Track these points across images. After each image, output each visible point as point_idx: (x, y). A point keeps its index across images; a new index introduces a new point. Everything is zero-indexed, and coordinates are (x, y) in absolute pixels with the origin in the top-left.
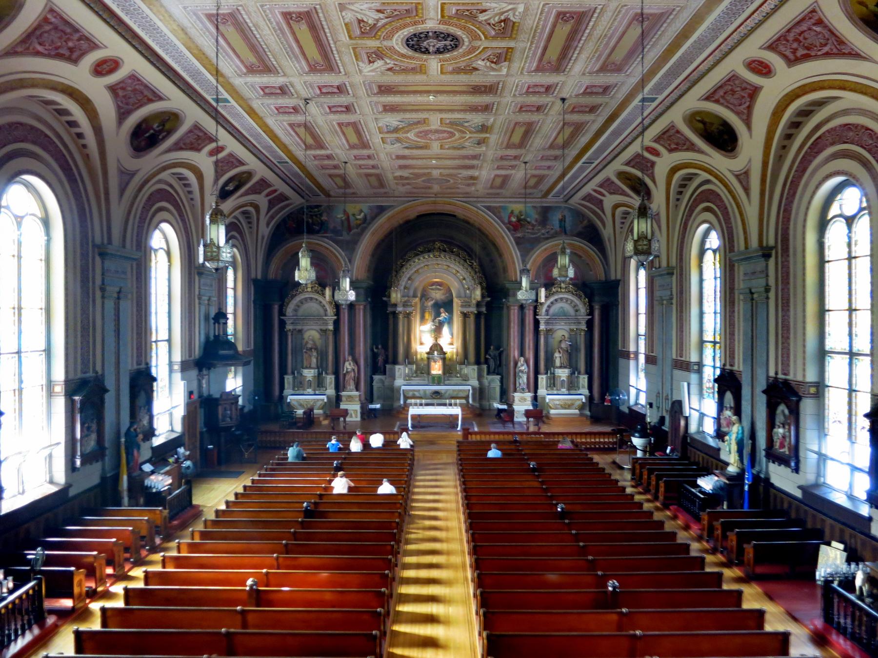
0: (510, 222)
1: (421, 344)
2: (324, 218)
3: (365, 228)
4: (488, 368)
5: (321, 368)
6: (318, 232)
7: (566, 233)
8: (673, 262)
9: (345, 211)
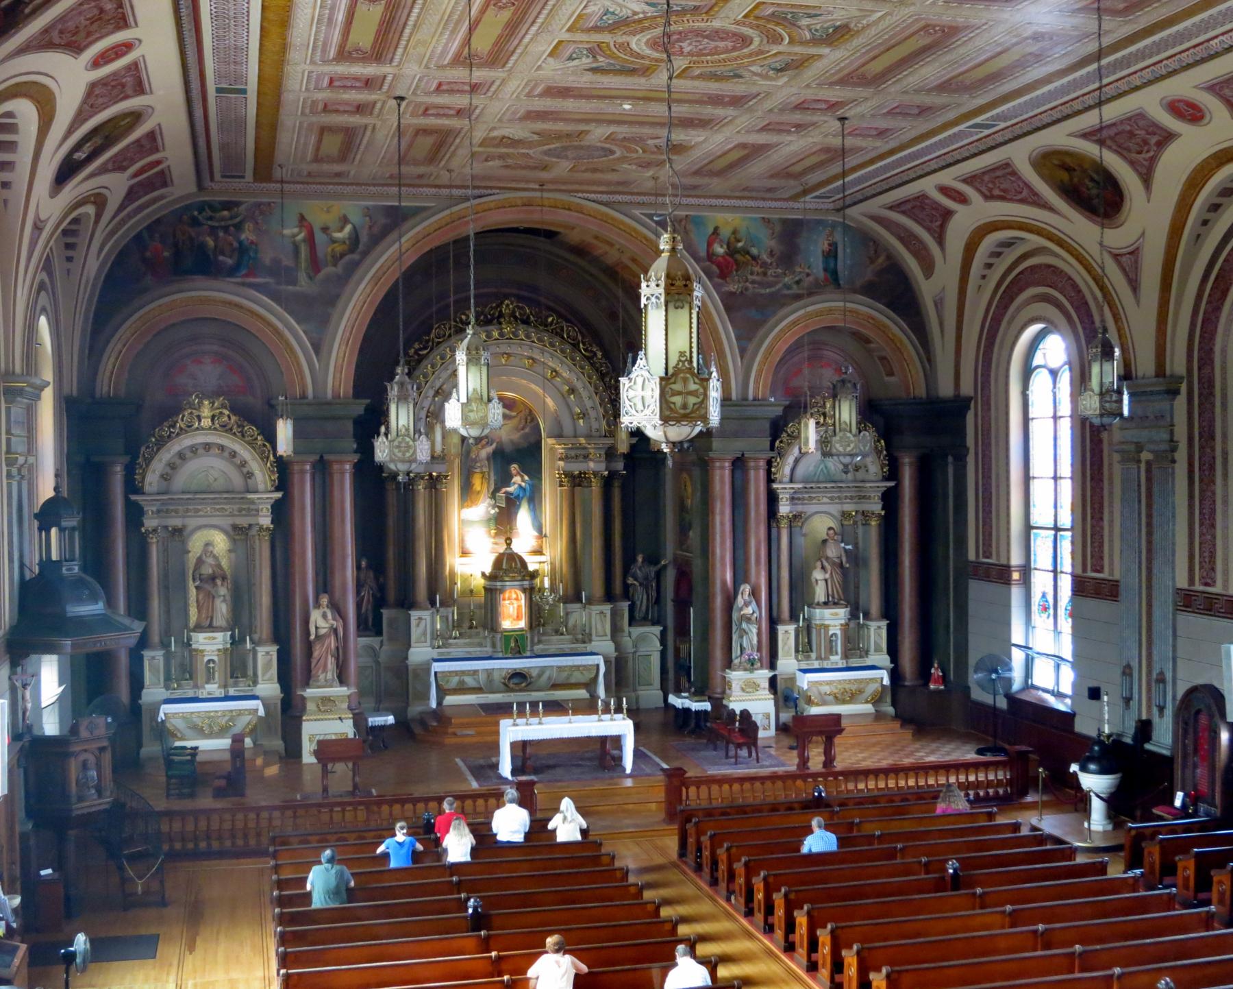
0: (710, 256)
1: (464, 553)
2: (247, 235)
3: (355, 265)
4: (632, 609)
5: (240, 626)
6: (232, 271)
7: (838, 286)
8: (1177, 363)
9: (302, 218)
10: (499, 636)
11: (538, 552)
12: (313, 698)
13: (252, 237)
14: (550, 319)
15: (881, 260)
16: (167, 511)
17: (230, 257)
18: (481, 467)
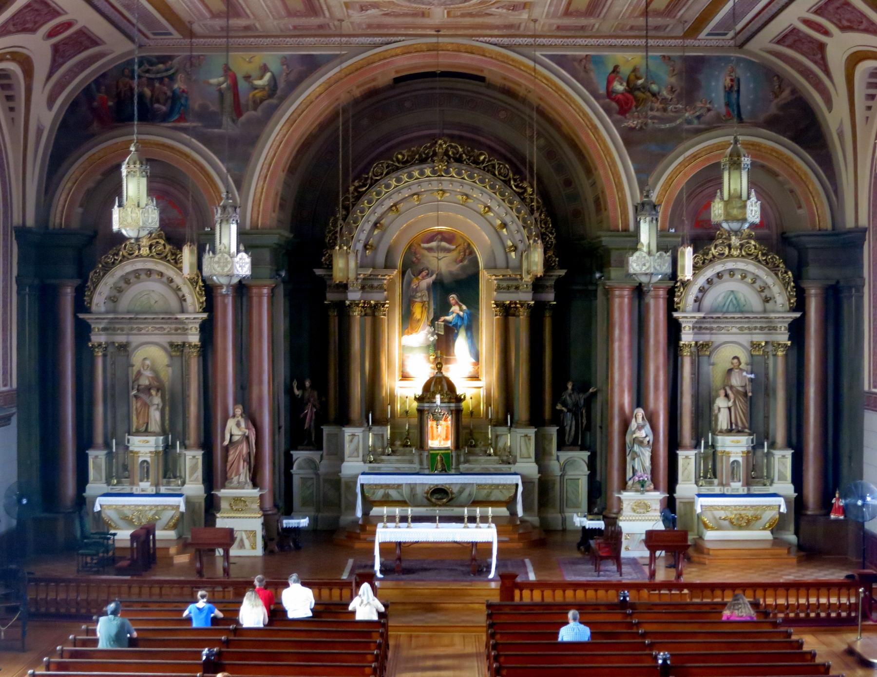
0: (610, 93)
1: (405, 377)
4: (561, 434)
5: (173, 434)
9: (227, 69)
10: (426, 454)
11: (475, 377)
12: (226, 498)
13: (184, 87)
14: (482, 158)
15: (786, 94)
16: (114, 329)
17: (164, 105)
18: (422, 297)
